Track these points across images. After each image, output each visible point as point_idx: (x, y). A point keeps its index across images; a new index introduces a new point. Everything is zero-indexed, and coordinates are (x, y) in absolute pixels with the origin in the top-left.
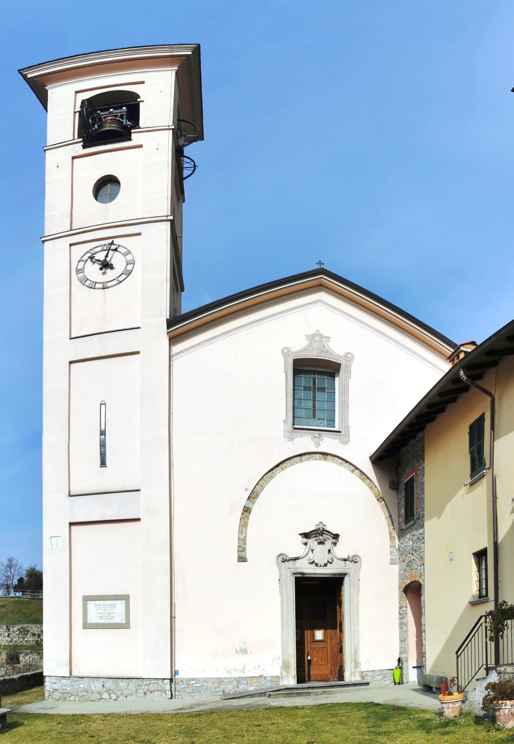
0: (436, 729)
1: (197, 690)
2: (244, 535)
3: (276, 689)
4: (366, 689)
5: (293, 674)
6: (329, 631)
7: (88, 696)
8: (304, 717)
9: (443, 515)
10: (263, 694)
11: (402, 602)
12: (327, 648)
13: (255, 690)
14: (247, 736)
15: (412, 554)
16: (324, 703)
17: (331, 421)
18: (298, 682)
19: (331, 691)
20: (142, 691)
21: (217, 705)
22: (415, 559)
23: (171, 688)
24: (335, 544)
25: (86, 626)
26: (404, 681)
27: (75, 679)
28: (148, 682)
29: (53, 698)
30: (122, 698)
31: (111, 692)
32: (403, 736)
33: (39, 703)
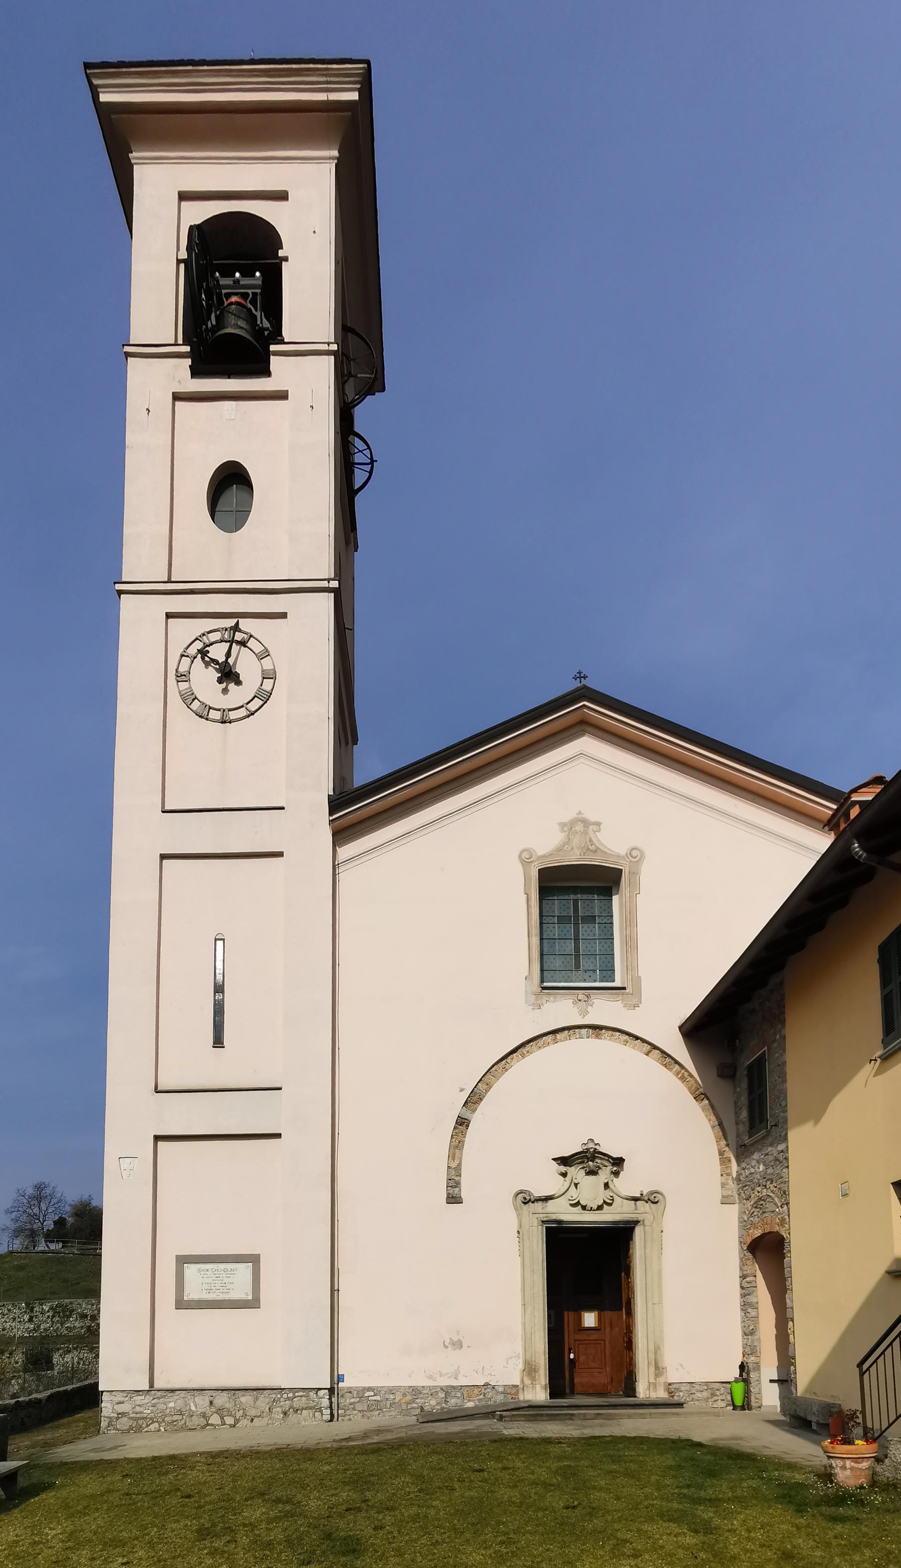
0: (818, 1506)
1: (377, 1406)
2: (457, 1162)
3: (513, 1406)
4: (677, 1414)
5: (543, 1383)
6: (608, 1314)
7: (183, 1422)
8: (560, 1458)
9: (824, 1119)
10: (489, 1414)
11: (745, 1268)
12: (604, 1341)
13: (476, 1407)
14: (458, 1490)
15: (765, 1186)
16: (597, 1434)
17: (608, 972)
18: (552, 1396)
19: (611, 1414)
20: (279, 1410)
21: (410, 1433)
22: (771, 1194)
23: (331, 1403)
24: (616, 1174)
25: (181, 1304)
26: (753, 1404)
27: (160, 1393)
28: (291, 1395)
29: (117, 1429)
30: (244, 1422)
31: (225, 1413)
32: (747, 1512)
33: (89, 1440)
